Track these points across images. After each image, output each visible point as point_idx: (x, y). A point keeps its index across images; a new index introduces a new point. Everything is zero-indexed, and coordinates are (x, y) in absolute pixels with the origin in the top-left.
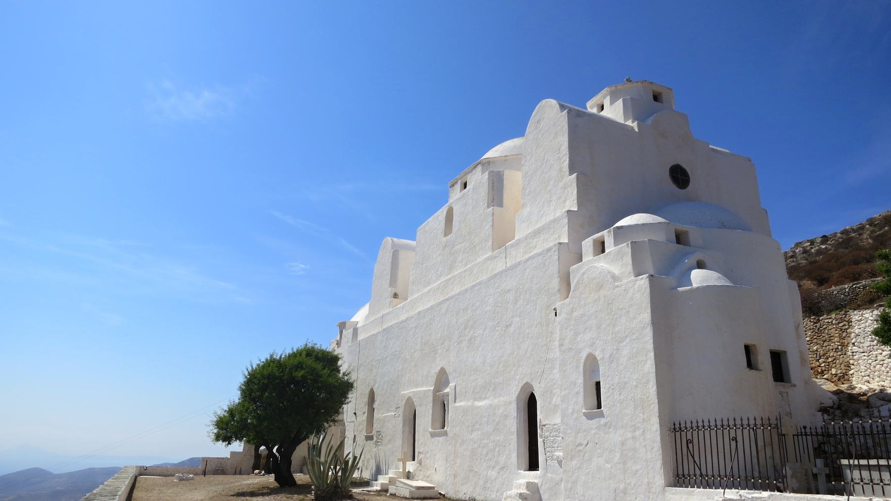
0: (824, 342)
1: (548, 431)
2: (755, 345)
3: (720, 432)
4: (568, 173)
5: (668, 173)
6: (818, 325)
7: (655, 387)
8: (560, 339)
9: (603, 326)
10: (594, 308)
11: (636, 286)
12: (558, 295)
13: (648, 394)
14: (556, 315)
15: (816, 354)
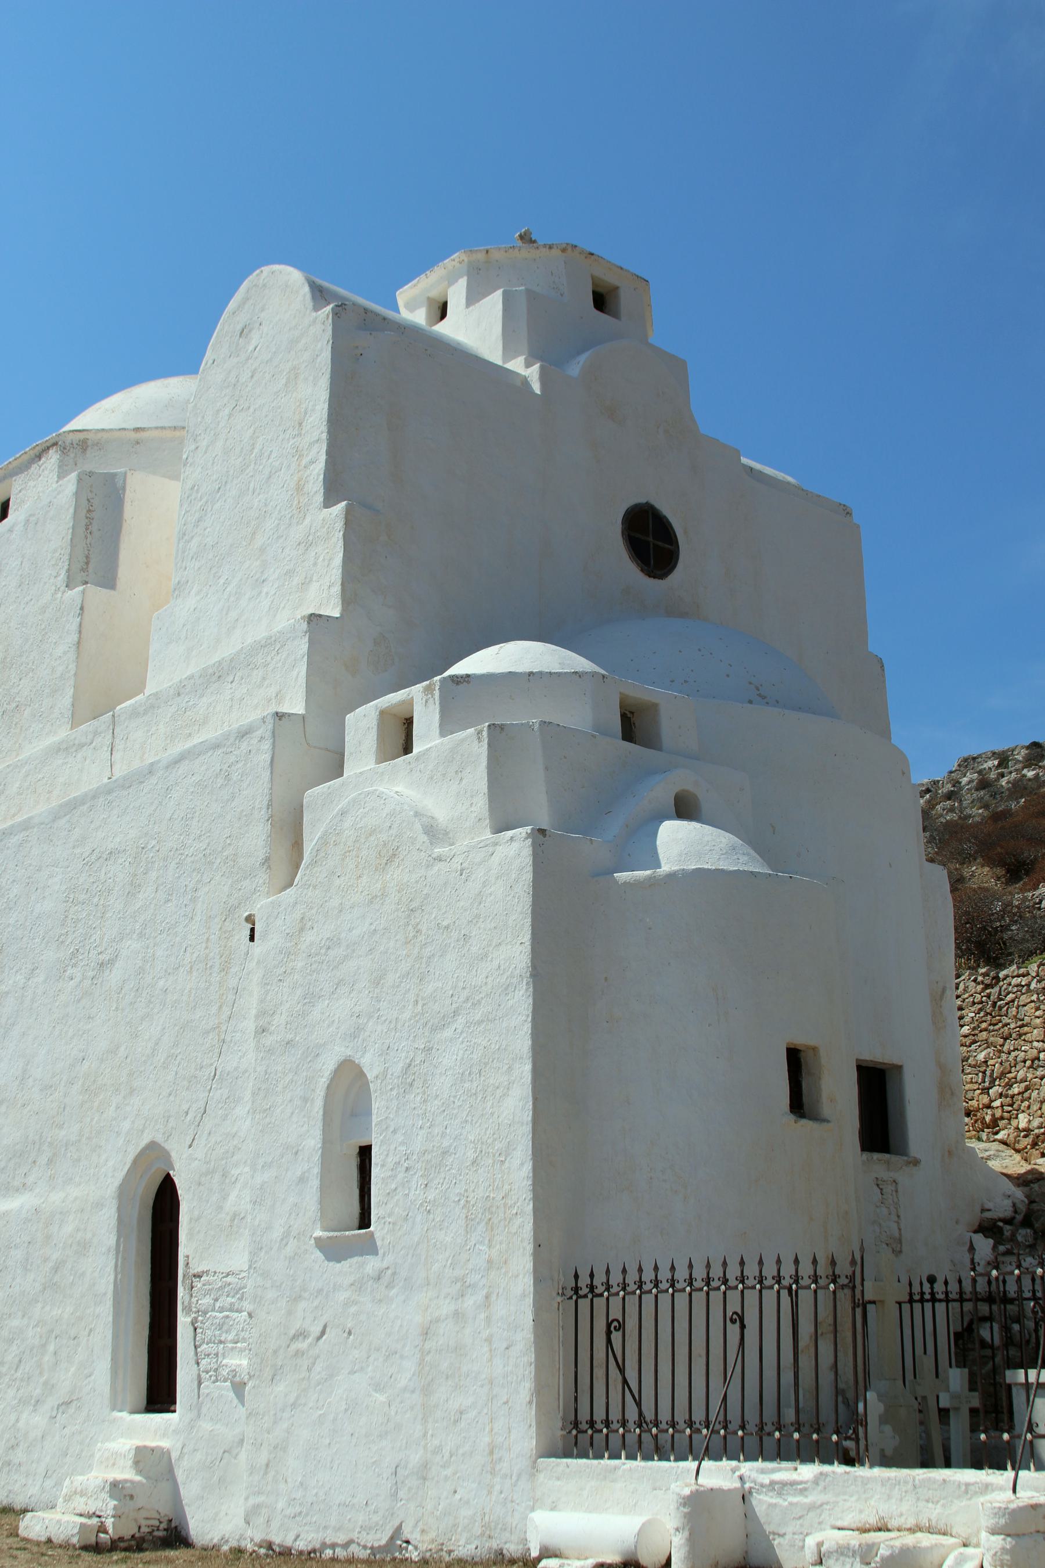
0: (1005, 1039)
1: (208, 1292)
2: (814, 1049)
3: (699, 1298)
4: (320, 498)
7: (528, 1166)
8: (261, 1014)
11: (496, 859)
12: (262, 877)
13: (507, 1187)
14: (252, 938)
15: (984, 1072)
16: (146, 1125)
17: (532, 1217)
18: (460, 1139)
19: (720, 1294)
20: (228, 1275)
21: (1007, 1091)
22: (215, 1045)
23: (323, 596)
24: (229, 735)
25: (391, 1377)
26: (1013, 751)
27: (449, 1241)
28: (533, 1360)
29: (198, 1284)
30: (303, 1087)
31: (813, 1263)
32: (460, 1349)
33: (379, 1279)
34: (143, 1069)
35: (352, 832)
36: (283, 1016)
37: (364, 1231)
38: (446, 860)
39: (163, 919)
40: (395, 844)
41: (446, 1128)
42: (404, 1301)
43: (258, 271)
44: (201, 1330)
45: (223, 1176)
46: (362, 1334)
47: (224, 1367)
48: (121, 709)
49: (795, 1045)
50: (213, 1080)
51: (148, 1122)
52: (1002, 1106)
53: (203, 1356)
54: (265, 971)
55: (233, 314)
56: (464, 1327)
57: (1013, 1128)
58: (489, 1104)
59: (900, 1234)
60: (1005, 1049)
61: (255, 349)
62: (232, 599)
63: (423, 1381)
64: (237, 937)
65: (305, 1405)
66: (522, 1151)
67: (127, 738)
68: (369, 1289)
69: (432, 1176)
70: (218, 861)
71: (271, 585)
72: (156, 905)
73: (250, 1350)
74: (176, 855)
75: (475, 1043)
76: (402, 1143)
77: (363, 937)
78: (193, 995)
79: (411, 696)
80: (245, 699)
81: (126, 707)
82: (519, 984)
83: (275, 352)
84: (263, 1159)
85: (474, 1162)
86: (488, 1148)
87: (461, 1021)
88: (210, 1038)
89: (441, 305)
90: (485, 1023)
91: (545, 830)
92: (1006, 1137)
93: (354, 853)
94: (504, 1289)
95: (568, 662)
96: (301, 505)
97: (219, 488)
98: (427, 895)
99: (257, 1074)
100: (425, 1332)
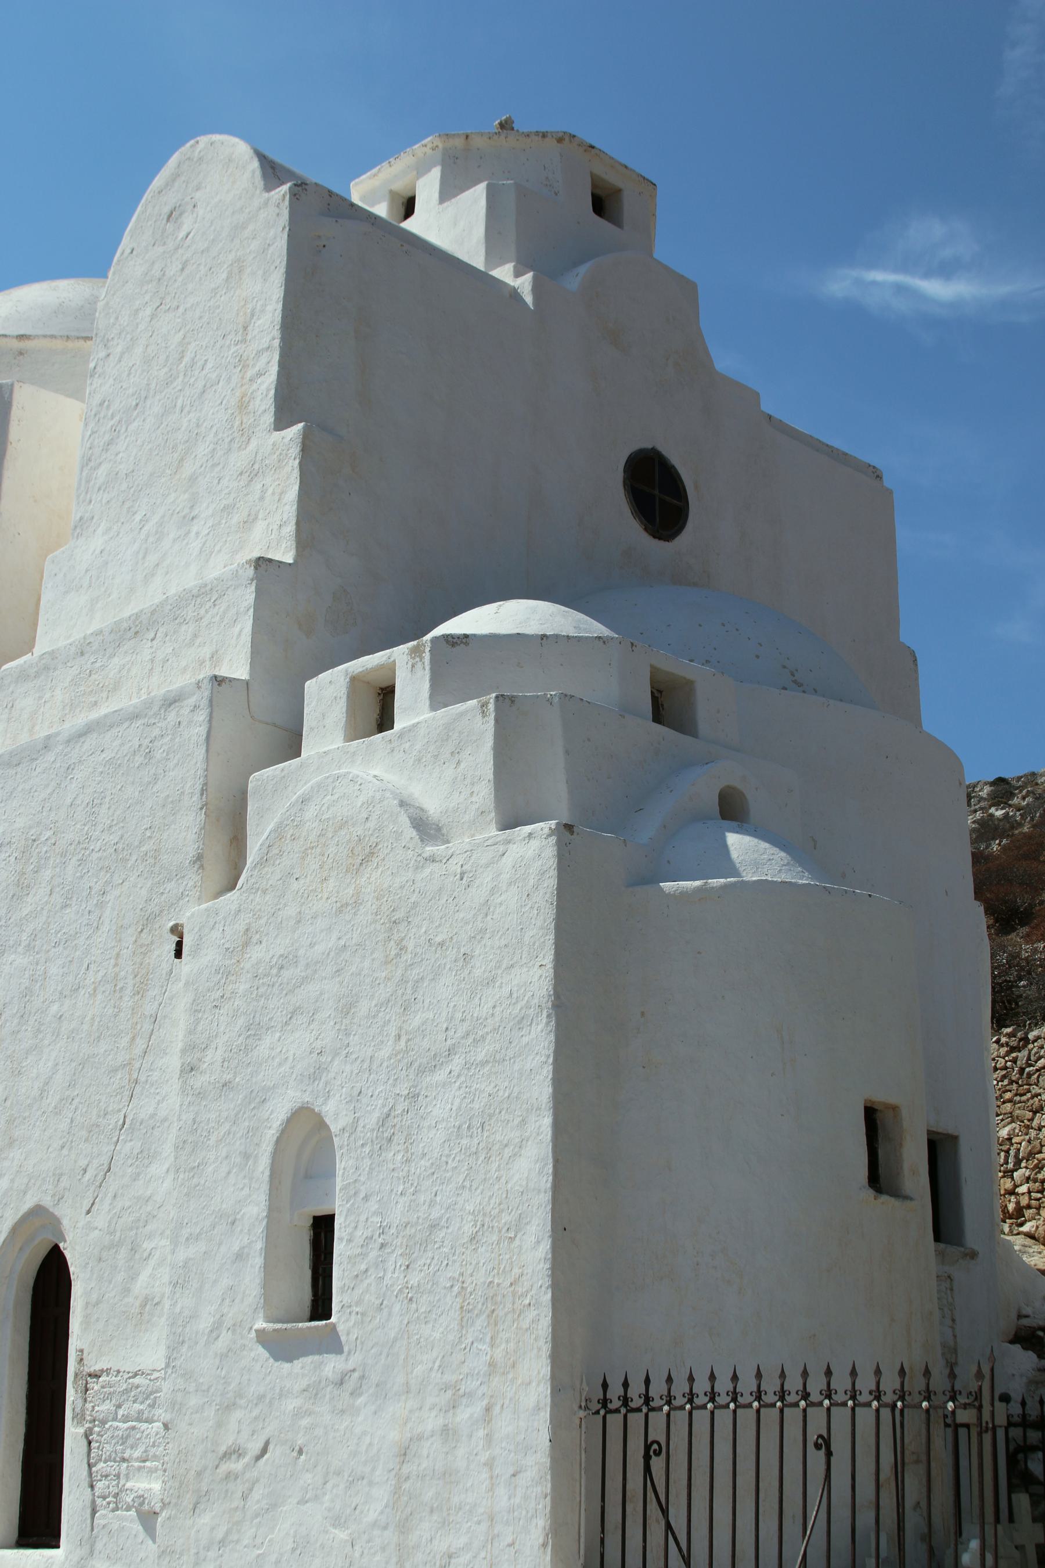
0: (1035, 1113)
1: (109, 1396)
2: (895, 1108)
3: (770, 1416)
4: (269, 418)
5: (619, 475)
6: (1023, 1055)
7: (546, 1246)
8: (189, 1048)
9: (364, 1007)
10: (335, 935)
11: (508, 861)
12: (192, 878)
13: (516, 1271)
14: (178, 954)
15: (1007, 1152)
16: (30, 1184)
17: (550, 1310)
18: (454, 1210)
19: (706, 1414)
20: (136, 1375)
21: (1036, 1174)
22: (124, 1087)
23: (273, 537)
24: (152, 703)
25: (355, 1509)
26: (975, 786)
27: (438, 1337)
28: (549, 1491)
29: (95, 1386)
30: (243, 1140)
31: (710, 1379)
32: (450, 1475)
33: (341, 1384)
34: (27, 1114)
35: (315, 824)
36: (219, 1051)
37: (324, 1322)
38: (441, 861)
39: (58, 929)
40: (374, 839)
41: (436, 1195)
42: (375, 1413)
43: (192, 142)
44: (98, 1444)
45: (132, 1250)
46: (318, 1454)
47: (128, 1492)
48: (5, 670)
49: (874, 1102)
50: (121, 1130)
51: (33, 1181)
52: (1029, 1192)
53: (99, 1477)
54: (196, 995)
55: (159, 193)
56: (455, 1447)
57: (1042, 1219)
58: (495, 1166)
59: (956, 1342)
60: (1035, 1123)
61: (187, 237)
62: (151, 539)
63: (399, 1513)
64: (156, 953)
65: (238, 1541)
66: (538, 1225)
67: (12, 706)
68: (328, 1396)
69: (415, 1255)
70: (134, 858)
71: (203, 523)
72: (49, 911)
73: (165, 1471)
74: (78, 850)
75: (476, 1090)
76: (376, 1213)
77: (328, 954)
78: (96, 1023)
79: (392, 659)
80: (170, 661)
81: (12, 668)
82: (537, 1017)
83: (213, 240)
84: (189, 1230)
85: (472, 1239)
86: (492, 1221)
87: (457, 1061)
88: (118, 1077)
89: (405, 201)
90: (490, 1065)
91: (573, 826)
92: (1034, 1229)
93: (318, 850)
94: (511, 1399)
95: (585, 626)
96: (244, 426)
97: (137, 405)
98: (415, 904)
99: (181, 1122)
100: (403, 1452)
